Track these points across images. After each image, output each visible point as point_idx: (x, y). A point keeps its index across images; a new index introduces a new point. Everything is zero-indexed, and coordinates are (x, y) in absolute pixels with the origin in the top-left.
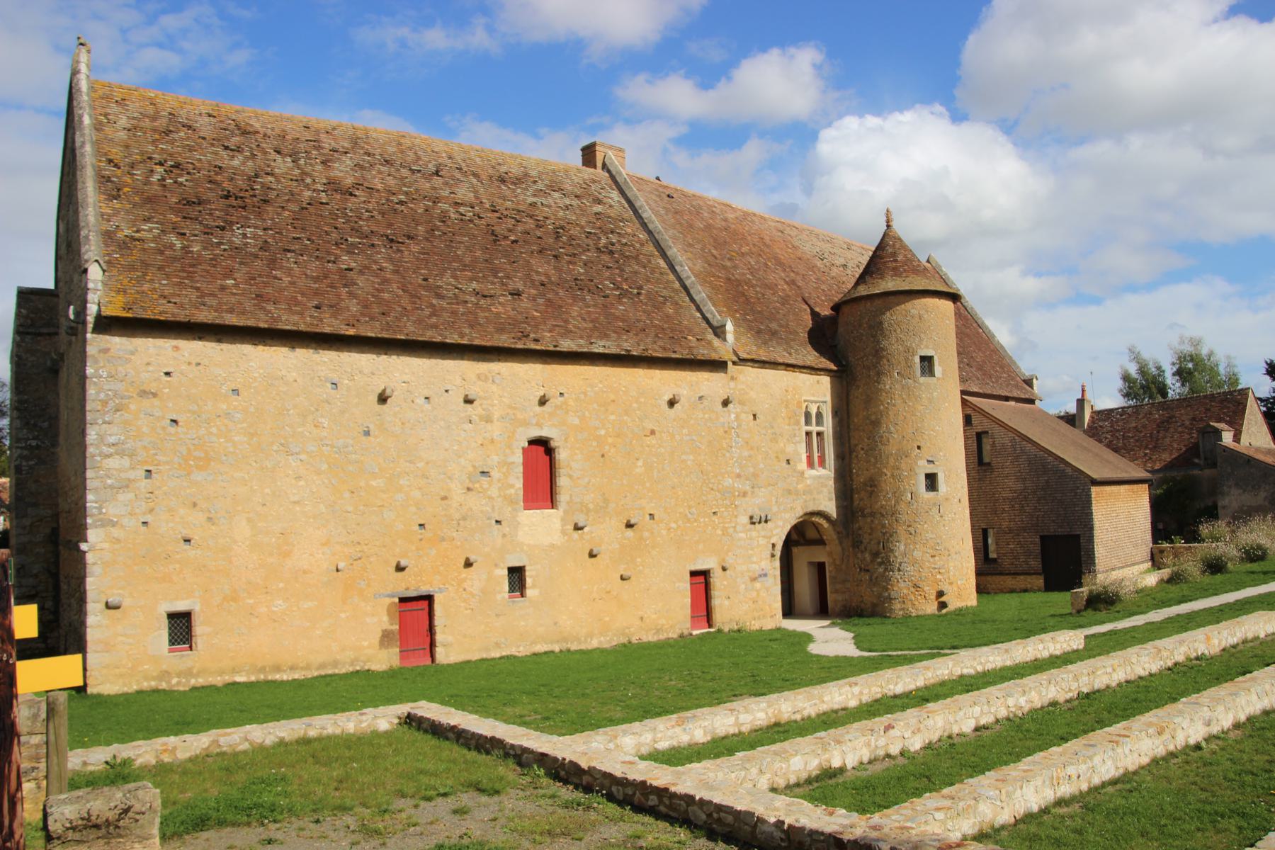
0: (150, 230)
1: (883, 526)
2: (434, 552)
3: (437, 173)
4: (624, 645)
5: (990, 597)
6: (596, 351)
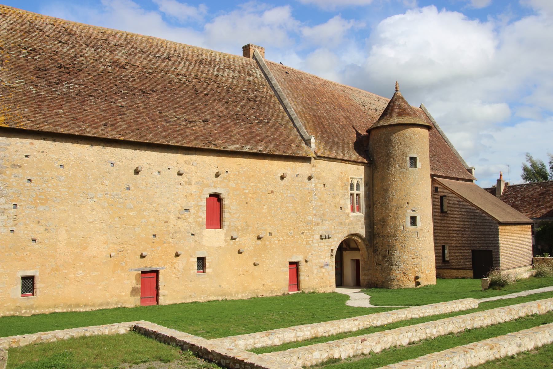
0: (19, 83)
1: (389, 242)
2: (160, 249)
3: (168, 59)
4: (254, 298)
5: (444, 280)
6: (245, 151)
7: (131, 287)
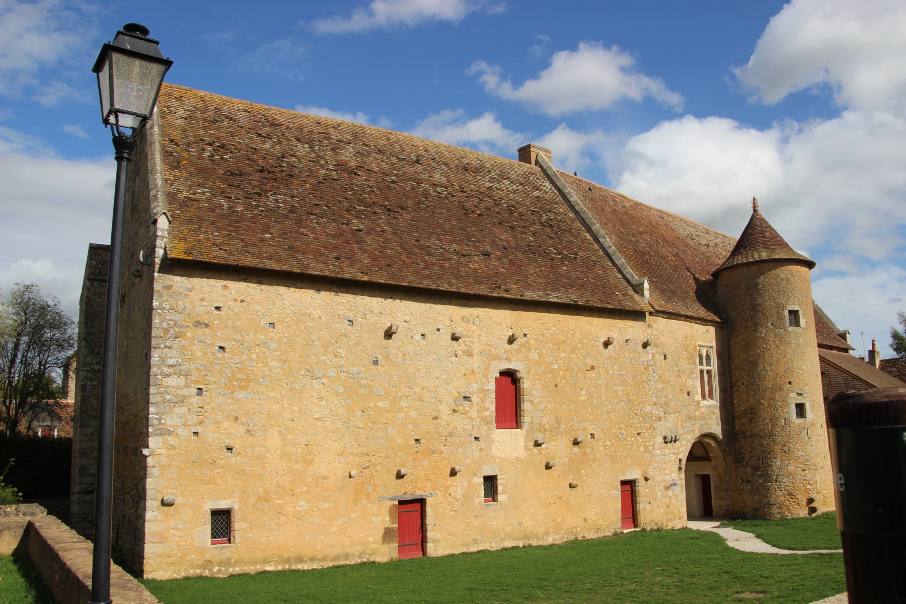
0: (204, 193)
1: (762, 446)
3: (417, 162)
7: (383, 527)
